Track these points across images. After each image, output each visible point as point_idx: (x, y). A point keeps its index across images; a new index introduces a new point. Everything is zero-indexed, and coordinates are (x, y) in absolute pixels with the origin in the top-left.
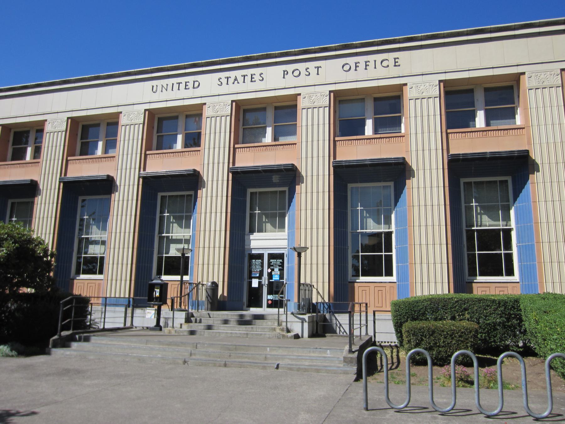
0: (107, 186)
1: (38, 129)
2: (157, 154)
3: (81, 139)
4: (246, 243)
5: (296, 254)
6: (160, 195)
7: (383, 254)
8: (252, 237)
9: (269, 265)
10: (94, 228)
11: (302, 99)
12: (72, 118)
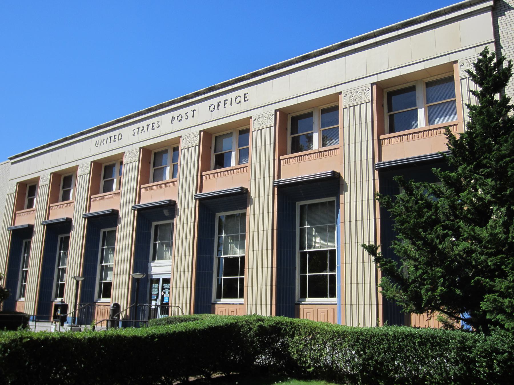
0: (241, 198)
1: (242, 131)
2: (291, 158)
3: (292, 134)
4: (149, 270)
5: (75, 281)
6: (299, 204)
7: (307, 274)
8: (153, 264)
9: (163, 289)
10: (233, 246)
11: (459, 67)
12: (280, 110)
